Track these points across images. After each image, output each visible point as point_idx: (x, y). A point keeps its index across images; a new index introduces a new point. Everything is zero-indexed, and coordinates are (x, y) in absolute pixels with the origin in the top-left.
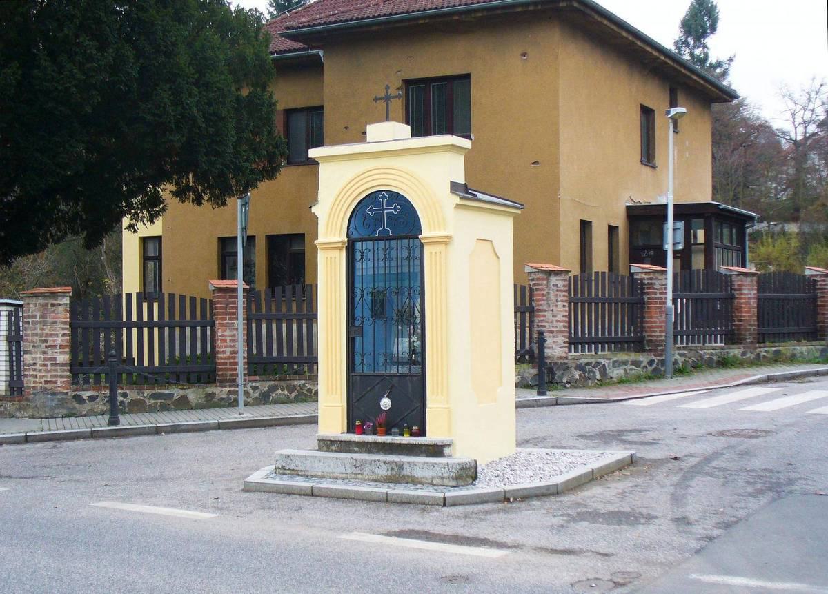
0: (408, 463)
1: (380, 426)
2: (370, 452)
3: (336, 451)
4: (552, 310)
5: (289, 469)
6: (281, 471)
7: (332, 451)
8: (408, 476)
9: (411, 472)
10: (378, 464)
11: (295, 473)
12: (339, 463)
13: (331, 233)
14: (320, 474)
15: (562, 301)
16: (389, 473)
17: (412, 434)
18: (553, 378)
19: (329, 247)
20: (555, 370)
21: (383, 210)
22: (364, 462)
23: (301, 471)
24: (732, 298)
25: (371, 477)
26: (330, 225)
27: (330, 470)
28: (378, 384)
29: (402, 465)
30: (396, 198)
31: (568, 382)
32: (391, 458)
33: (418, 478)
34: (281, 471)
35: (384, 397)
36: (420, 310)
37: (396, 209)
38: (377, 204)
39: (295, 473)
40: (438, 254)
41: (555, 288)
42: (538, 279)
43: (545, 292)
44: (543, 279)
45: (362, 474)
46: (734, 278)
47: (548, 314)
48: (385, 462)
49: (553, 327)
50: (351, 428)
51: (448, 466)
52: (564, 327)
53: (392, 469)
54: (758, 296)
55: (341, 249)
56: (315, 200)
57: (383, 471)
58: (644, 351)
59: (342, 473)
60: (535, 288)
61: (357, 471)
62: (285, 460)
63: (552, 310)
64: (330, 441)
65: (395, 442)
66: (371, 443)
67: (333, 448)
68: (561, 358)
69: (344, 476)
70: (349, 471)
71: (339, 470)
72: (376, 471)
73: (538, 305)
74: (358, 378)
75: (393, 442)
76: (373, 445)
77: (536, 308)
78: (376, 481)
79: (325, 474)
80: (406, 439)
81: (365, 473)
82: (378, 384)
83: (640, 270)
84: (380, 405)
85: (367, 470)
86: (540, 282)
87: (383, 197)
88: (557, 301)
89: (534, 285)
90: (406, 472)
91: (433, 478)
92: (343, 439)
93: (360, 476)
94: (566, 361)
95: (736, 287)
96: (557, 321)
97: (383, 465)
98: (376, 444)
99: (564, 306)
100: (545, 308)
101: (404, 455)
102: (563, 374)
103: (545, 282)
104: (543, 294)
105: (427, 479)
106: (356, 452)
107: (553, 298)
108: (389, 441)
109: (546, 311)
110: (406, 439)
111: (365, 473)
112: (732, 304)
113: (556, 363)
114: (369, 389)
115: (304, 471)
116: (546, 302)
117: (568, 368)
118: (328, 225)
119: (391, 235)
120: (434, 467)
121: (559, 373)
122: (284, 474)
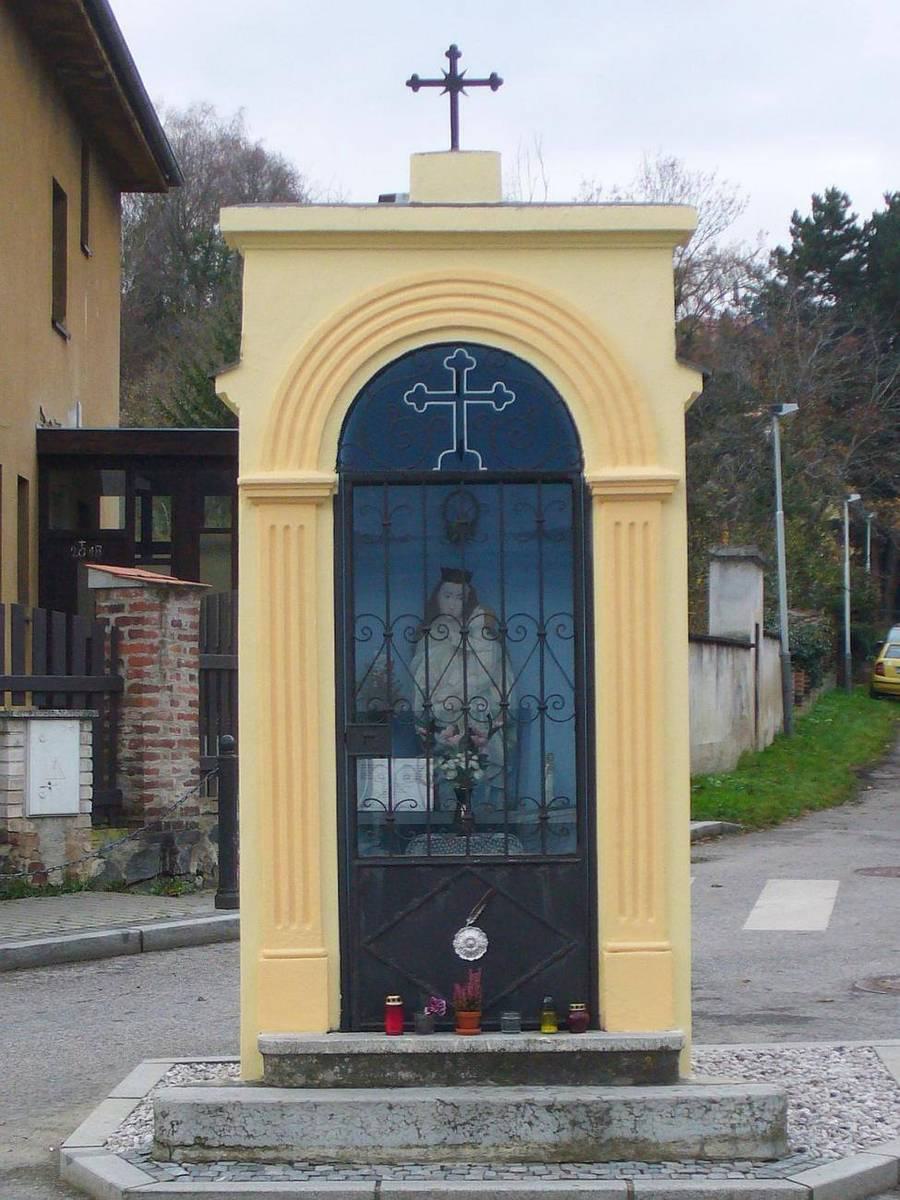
0: (626, 1104)
1: (471, 1005)
2: (452, 1081)
3: (337, 1085)
4: (170, 688)
5: (222, 1147)
6: (193, 1154)
7: (322, 1085)
8: (626, 1141)
9: (634, 1130)
10: (529, 1112)
11: (245, 1155)
12: (397, 1117)
14: (332, 1153)
15: (188, 665)
16: (566, 1136)
17: (567, 1026)
18: (173, 863)
19: (277, 496)
20: (176, 840)
22: (484, 1111)
23: (265, 1148)
25: (506, 1152)
26: (284, 435)
27: (370, 1141)
28: (445, 888)
29: (609, 1110)
31: (199, 873)
32: (565, 1094)
33: (656, 1145)
34: (193, 1154)
35: (463, 925)
36: (572, 679)
37: (499, 397)
38: (440, 380)
39: (245, 1155)
41: (176, 631)
42: (134, 607)
43: (156, 642)
44: (151, 608)
45: (474, 1146)
47: (163, 697)
48: (550, 1108)
49: (172, 730)
50: (357, 1011)
52: (193, 731)
53: (574, 1123)
54: (202, 661)
55: (318, 503)
56: (229, 352)
57: (544, 1133)
59: (408, 1147)
60: (125, 629)
61: (454, 1137)
62: (207, 1120)
63: (170, 688)
64: (318, 1056)
65: (539, 1048)
66: (453, 1056)
67: (329, 1076)
68: (188, 811)
69: (414, 1153)
70: (432, 1139)
71: (397, 1138)
72: (521, 1132)
73: (139, 675)
74: (379, 874)
75: (532, 1048)
76: (462, 1061)
77: (127, 684)
78: (523, 1161)
79: (350, 1152)
80: (549, 1040)
81: (487, 1141)
82: (445, 888)
83: (114, 583)
84: (453, 949)
85: (491, 1136)
86: (146, 614)
87: (459, 363)
88: (179, 665)
89: (125, 621)
90: (622, 1127)
91: (704, 1141)
92: (364, 1050)
93: (468, 1152)
94: (195, 819)
96: (181, 717)
97: (545, 1116)
98: (472, 1057)
99: (192, 677)
100: (155, 682)
101: (565, 1083)
102: (190, 851)
103: (156, 615)
104: (151, 646)
105: (686, 1145)
106: (403, 1084)
107: (172, 656)
108: (516, 1048)
109: (156, 689)
110: (549, 1040)
111: (487, 1141)
113: (179, 824)
114: (416, 901)
115: (275, 1148)
116: (157, 667)
117: (198, 837)
118: (276, 435)
119: (481, 469)
121: (183, 850)
122: (206, 1162)
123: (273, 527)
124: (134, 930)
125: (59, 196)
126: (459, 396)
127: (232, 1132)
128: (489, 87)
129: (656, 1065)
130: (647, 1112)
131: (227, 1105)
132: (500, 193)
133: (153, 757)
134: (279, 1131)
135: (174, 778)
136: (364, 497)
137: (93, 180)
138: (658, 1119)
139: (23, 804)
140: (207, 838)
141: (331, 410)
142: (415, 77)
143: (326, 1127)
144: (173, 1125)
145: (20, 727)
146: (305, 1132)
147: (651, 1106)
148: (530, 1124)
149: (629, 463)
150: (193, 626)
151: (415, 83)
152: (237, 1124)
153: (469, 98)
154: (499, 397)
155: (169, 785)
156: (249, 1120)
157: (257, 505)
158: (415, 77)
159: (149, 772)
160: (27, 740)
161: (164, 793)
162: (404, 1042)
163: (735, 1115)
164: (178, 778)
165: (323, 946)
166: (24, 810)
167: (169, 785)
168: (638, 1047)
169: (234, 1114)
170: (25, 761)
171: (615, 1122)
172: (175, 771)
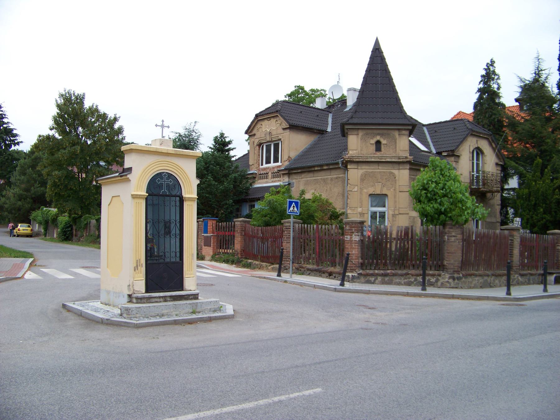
21: (165, 181)
30: (170, 176)
37: (171, 182)
87: (165, 175)
151: (156, 125)
153: (165, 129)
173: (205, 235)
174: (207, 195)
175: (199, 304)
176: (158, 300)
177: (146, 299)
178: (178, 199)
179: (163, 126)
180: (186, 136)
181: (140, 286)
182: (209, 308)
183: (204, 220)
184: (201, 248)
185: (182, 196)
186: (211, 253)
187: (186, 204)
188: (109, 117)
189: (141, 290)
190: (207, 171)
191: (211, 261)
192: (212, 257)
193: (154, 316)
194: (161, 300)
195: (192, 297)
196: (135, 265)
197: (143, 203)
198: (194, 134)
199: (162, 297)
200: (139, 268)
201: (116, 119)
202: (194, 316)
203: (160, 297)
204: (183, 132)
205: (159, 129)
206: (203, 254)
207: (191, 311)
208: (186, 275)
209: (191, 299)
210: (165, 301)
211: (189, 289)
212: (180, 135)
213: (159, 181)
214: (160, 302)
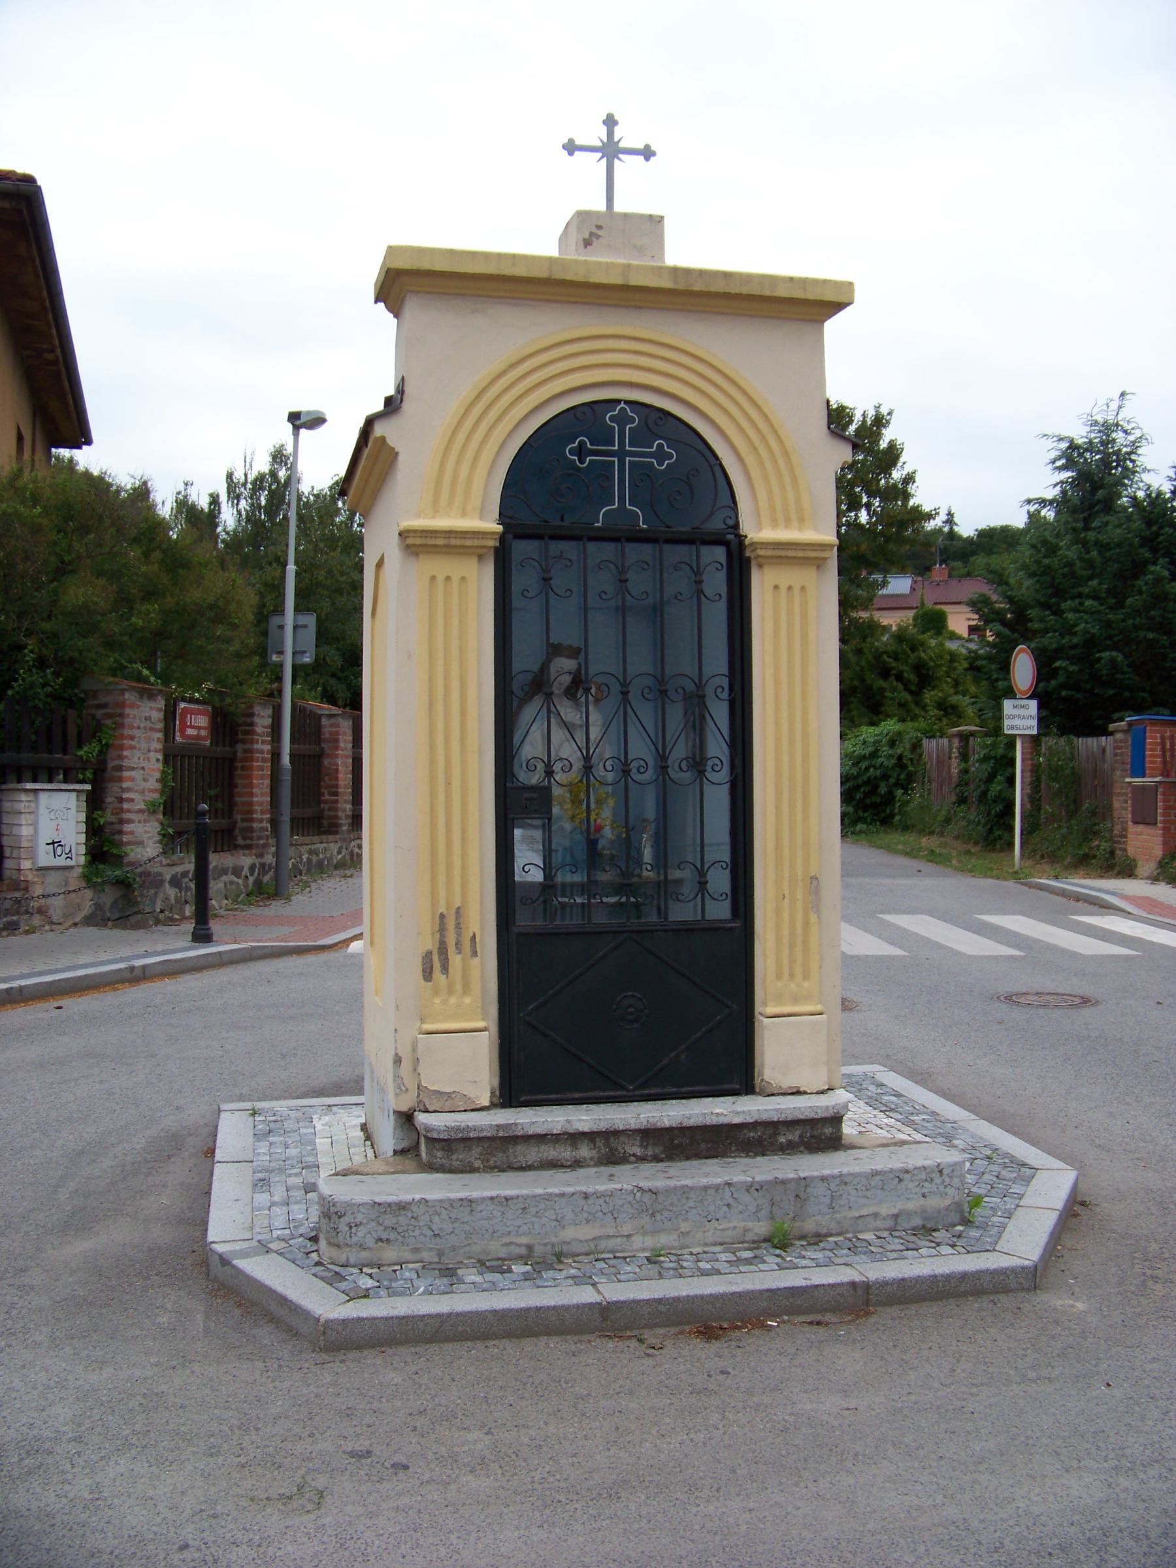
4: (143, 768)
13: (450, 503)
21: (621, 454)
24: (320, 755)
30: (656, 422)
31: (162, 911)
37: (661, 455)
40: (796, 591)
46: (324, 721)
48: (749, 1187)
50: (514, 1088)
51: (941, 1172)
58: (236, 847)
62: (389, 1220)
63: (143, 768)
87: (622, 419)
95: (327, 735)
97: (746, 1198)
99: (158, 760)
112: (319, 765)
118: (438, 483)
120: (900, 1180)
123: (433, 578)
124: (138, 963)
125: (20, 439)
126: (621, 454)
127: (417, 1233)
128: (642, 158)
129: (822, 1134)
130: (843, 1187)
131: (411, 1204)
132: (662, 259)
133: (130, 821)
134: (467, 1228)
135: (145, 837)
136: (521, 549)
137: (38, 435)
138: (854, 1192)
139: (33, 857)
140: (167, 885)
141: (494, 461)
142: (571, 141)
143: (519, 1222)
144: (351, 1227)
145: (31, 797)
146: (496, 1228)
147: (846, 1180)
148: (728, 1205)
149: (787, 527)
150: (160, 721)
151: (571, 148)
152: (422, 1223)
153: (626, 167)
154: (661, 455)
155: (141, 843)
156: (436, 1219)
157: (417, 554)
158: (571, 141)
159: (127, 833)
160: (37, 807)
161: (139, 850)
162: (580, 1120)
163: (926, 1184)
164: (149, 838)
165: (483, 1019)
166: (33, 863)
167: (141, 843)
168: (812, 1115)
169: (419, 1211)
170: (35, 825)
171: (812, 1199)
172: (146, 832)
173: (1138, 781)
174: (1150, 636)
175: (819, 1190)
176: (565, 1153)
177: (476, 1151)
178: (720, 553)
179: (610, 151)
180: (1090, 447)
181: (463, 1061)
182: (884, 1211)
183: (1130, 724)
184: (1125, 829)
185: (741, 538)
186: (1158, 852)
187: (764, 587)
188: (858, 417)
189: (471, 1092)
190: (1154, 550)
191: (1155, 879)
192: (1162, 865)
193: (495, 1265)
194: (584, 1151)
195: (794, 1136)
196: (429, 943)
197: (480, 583)
198: (1119, 436)
199: (590, 1137)
200: (455, 960)
201: (880, 422)
202: (769, 1276)
203: (574, 1138)
204: (1080, 433)
205: (595, 165)
206: (1131, 852)
207: (761, 1228)
208: (766, 1002)
209: (789, 1148)
210: (613, 1158)
211: (788, 1082)
212: (1073, 446)
213: (581, 452)
214: (577, 1164)
